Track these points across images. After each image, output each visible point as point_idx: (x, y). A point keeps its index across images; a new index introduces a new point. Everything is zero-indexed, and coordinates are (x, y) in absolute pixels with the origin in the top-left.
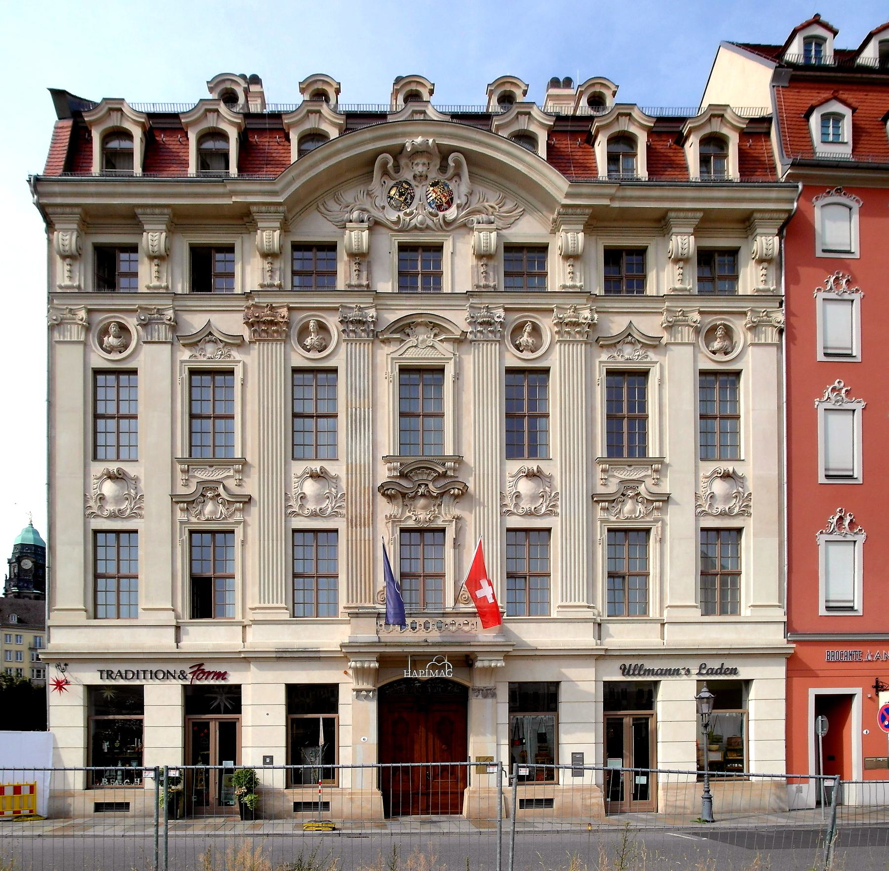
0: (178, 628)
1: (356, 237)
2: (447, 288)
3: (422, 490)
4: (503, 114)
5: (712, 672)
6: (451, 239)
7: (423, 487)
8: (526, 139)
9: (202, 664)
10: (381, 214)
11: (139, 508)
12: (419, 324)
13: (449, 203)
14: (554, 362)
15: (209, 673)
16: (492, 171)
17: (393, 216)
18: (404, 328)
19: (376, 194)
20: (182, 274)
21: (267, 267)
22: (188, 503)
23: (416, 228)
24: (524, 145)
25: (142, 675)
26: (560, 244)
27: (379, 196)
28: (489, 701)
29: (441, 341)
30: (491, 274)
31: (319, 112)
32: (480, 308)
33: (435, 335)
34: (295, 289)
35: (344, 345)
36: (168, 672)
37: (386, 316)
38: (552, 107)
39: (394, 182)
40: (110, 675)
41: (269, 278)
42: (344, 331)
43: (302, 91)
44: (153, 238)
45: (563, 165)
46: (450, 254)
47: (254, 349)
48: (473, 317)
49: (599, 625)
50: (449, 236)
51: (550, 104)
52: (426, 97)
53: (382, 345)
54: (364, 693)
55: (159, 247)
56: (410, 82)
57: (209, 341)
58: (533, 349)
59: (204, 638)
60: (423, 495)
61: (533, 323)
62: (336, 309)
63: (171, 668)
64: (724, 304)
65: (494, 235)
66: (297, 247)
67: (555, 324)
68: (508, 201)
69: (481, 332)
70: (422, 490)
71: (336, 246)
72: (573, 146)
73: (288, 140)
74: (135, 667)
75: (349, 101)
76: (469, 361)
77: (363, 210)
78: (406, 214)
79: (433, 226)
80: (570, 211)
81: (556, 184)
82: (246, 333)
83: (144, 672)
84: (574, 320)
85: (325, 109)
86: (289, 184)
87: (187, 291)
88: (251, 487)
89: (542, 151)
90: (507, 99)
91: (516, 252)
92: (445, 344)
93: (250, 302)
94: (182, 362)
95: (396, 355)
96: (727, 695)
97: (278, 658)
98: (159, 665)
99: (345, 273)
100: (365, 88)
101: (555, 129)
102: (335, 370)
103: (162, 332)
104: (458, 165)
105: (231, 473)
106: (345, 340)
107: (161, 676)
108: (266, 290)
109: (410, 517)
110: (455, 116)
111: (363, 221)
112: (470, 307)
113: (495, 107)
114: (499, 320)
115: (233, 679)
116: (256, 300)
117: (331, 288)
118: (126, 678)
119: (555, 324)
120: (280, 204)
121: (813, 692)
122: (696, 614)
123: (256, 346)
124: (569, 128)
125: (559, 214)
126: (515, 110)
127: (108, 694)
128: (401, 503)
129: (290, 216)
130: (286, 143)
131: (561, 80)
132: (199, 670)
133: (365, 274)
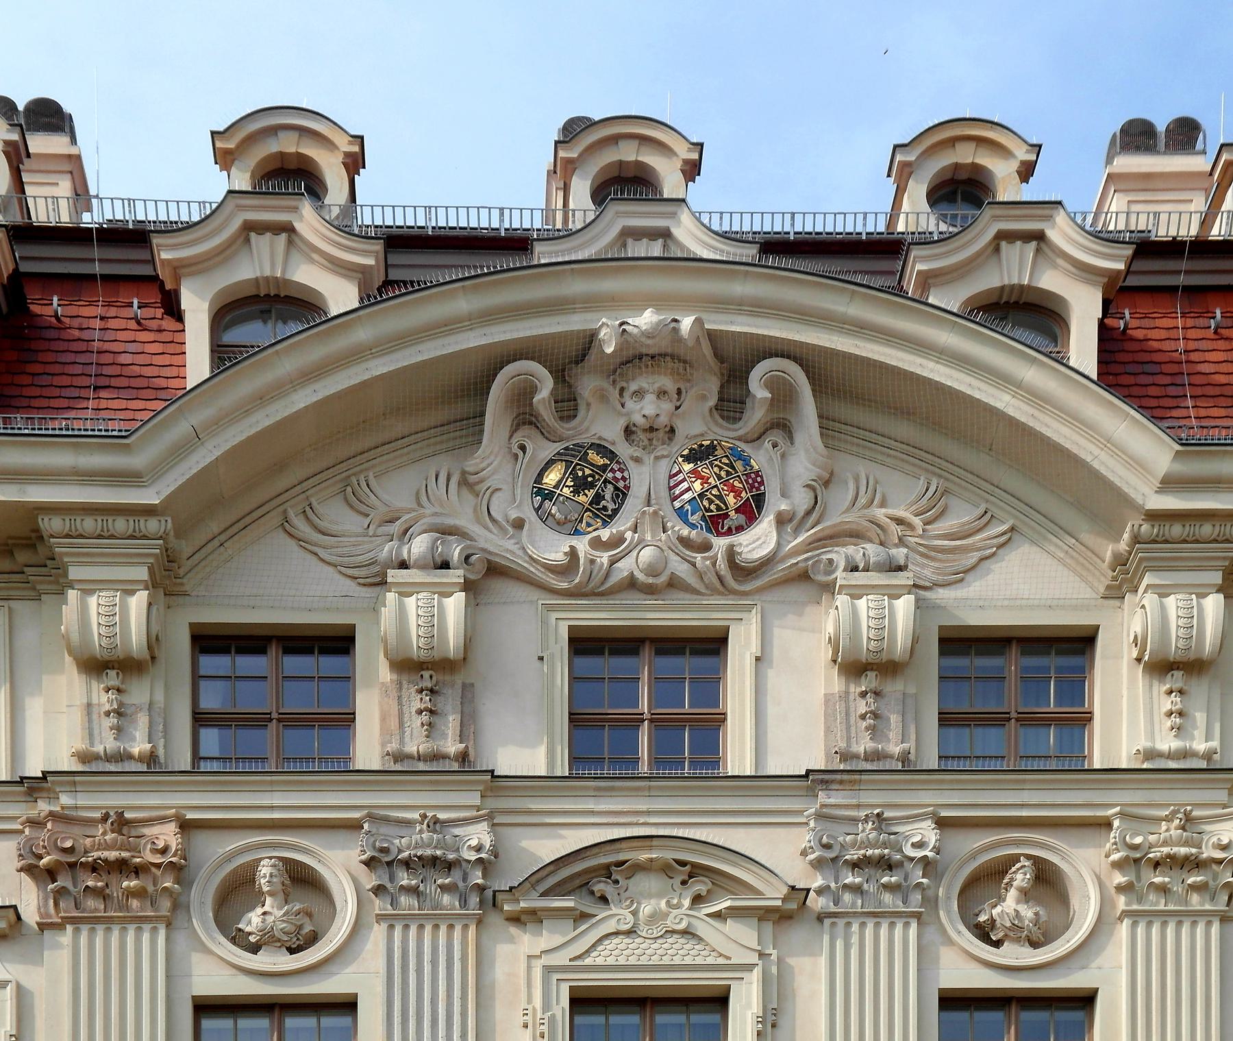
1: (424, 612)
2: (738, 756)
4: (944, 239)
8: (1027, 315)
10: (510, 544)
12: (639, 868)
13: (751, 511)
14: (1112, 974)
16: (904, 412)
17: (553, 548)
18: (589, 879)
19: (493, 482)
21: (105, 700)
23: (631, 584)
24: (1018, 333)
26: (1137, 627)
27: (502, 491)
29: (717, 916)
30: (894, 719)
31: (289, 229)
32: (855, 820)
33: (697, 900)
34: (204, 766)
35: (378, 933)
37: (525, 844)
38: (1121, 213)
39: (559, 447)
42: (379, 890)
43: (224, 159)
45: (1153, 391)
46: (749, 662)
47: (59, 946)
48: (827, 847)
51: (1117, 203)
52: (671, 181)
53: (513, 930)
56: (615, 139)
58: (1037, 935)
61: (1036, 860)
62: (355, 826)
65: (904, 606)
66: (208, 641)
67: (1117, 865)
68: (954, 502)
69: (856, 889)
71: (352, 639)
72: (1192, 334)
73: (178, 316)
75: (396, 192)
76: (813, 972)
77: (446, 531)
78: (597, 544)
79: (692, 580)
80: (1177, 530)
81: (1132, 452)
82: (30, 901)
84: (1183, 851)
85: (307, 220)
86: (179, 451)
89: (1083, 347)
90: (962, 191)
91: (979, 654)
92: (731, 927)
93: (44, 807)
95: (561, 959)
99: (384, 719)
100: (457, 151)
101: (1132, 281)
102: (348, 1006)
104: (783, 395)
106: (380, 918)
108: (95, 768)
110: (778, 248)
111: (445, 565)
112: (820, 816)
113: (916, 214)
114: (919, 854)
116: (65, 800)
117: (338, 767)
119: (1117, 865)
120: (148, 511)
123: (66, 937)
124: (1181, 280)
125: (1136, 539)
126: (988, 225)
129: (185, 548)
130: (169, 323)
131: (1161, 127)
133: (452, 723)
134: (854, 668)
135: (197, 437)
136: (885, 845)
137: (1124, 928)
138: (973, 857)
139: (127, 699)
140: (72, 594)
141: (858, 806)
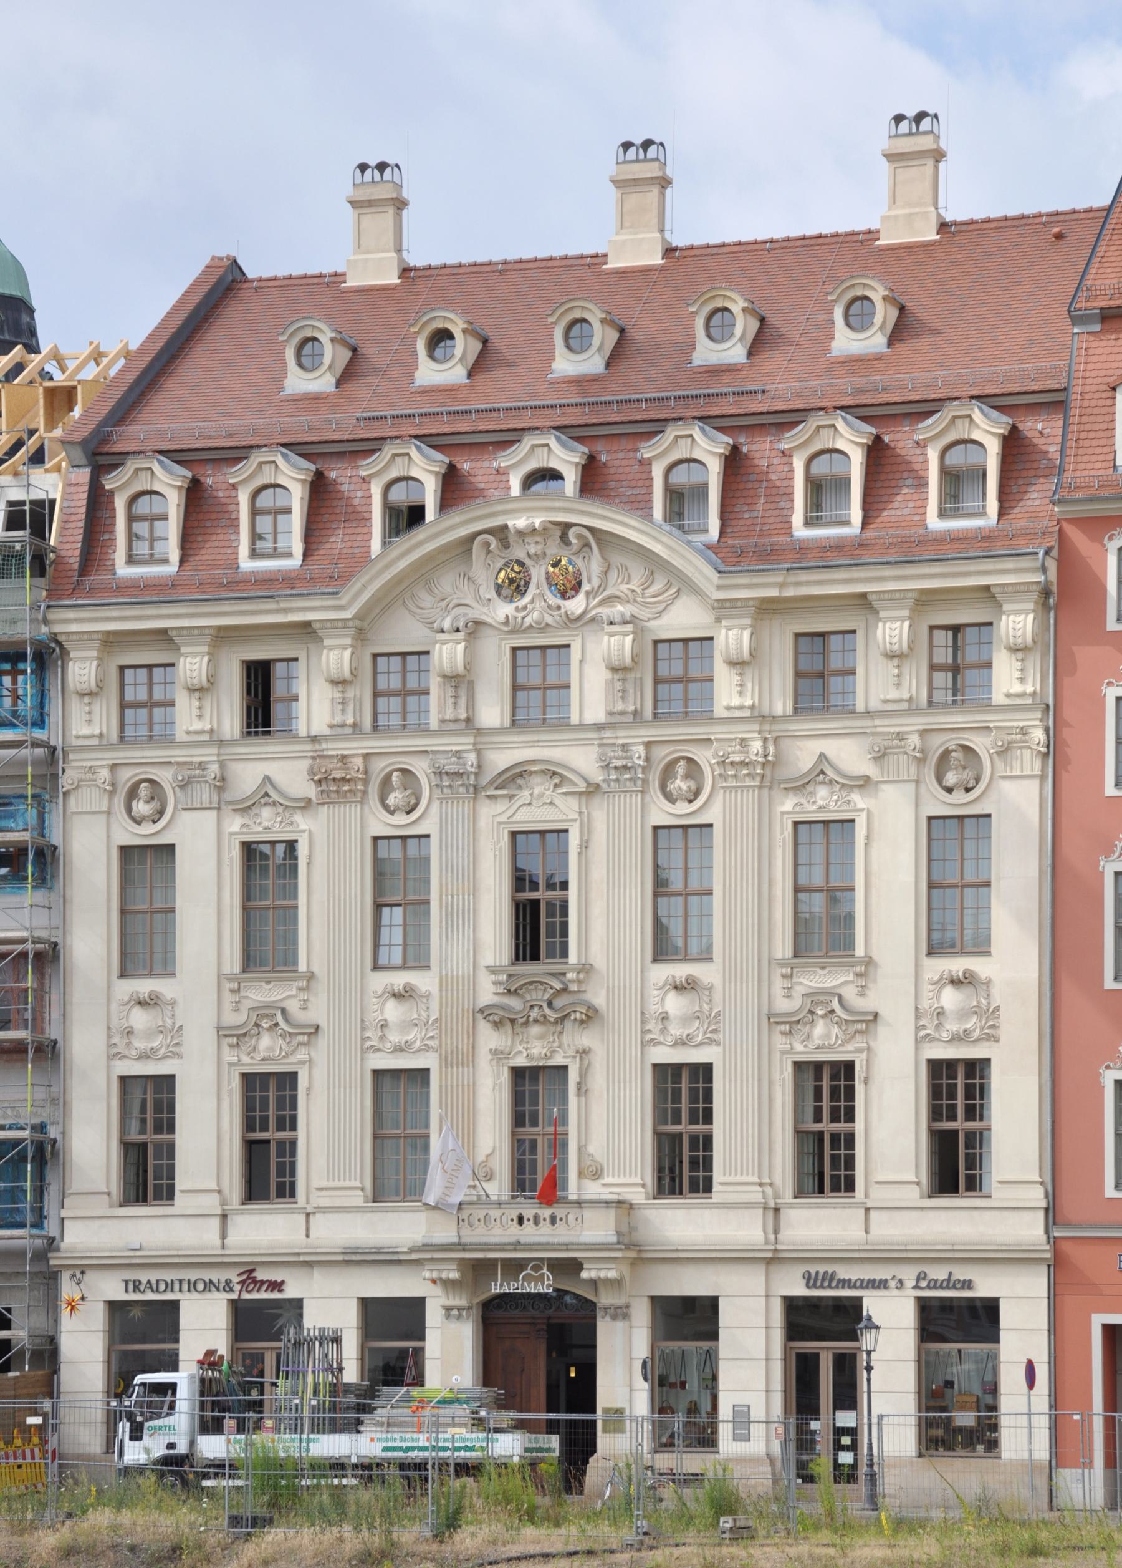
0: (224, 1217)
1: (448, 653)
3: (535, 1013)
5: (934, 1284)
6: (579, 640)
7: (536, 1009)
9: (253, 1270)
11: (177, 1044)
15: (262, 1282)
20: (232, 706)
22: (238, 1036)
25: (177, 1286)
28: (620, 1325)
33: (556, 786)
36: (211, 1281)
40: (136, 1288)
41: (339, 713)
44: (192, 665)
49: (777, 1210)
50: (577, 635)
54: (455, 1312)
55: (200, 674)
57: (265, 804)
59: (265, 1230)
60: (536, 1021)
63: (215, 1275)
64: (960, 719)
70: (535, 1013)
74: (169, 1275)
79: (554, 624)
83: (181, 1281)
87: (237, 733)
88: (317, 1013)
92: (569, 799)
94: (232, 834)
95: (503, 818)
96: (958, 1322)
97: (348, 1263)
98: (198, 1270)
103: (202, 794)
105: (294, 992)
107: (201, 1287)
109: (520, 1052)
111: (458, 630)
115: (983, 1289)
118: (157, 1291)
121: (1098, 1320)
122: (913, 1195)
127: (136, 1313)
128: (510, 1031)
129: (365, 624)
132: (250, 1279)
133: (463, 701)
134: (615, 670)
135: (364, 586)
136: (625, 758)
137: (722, 791)
138: (664, 758)
139: (346, 695)
140: (325, 652)
141: (617, 738)
